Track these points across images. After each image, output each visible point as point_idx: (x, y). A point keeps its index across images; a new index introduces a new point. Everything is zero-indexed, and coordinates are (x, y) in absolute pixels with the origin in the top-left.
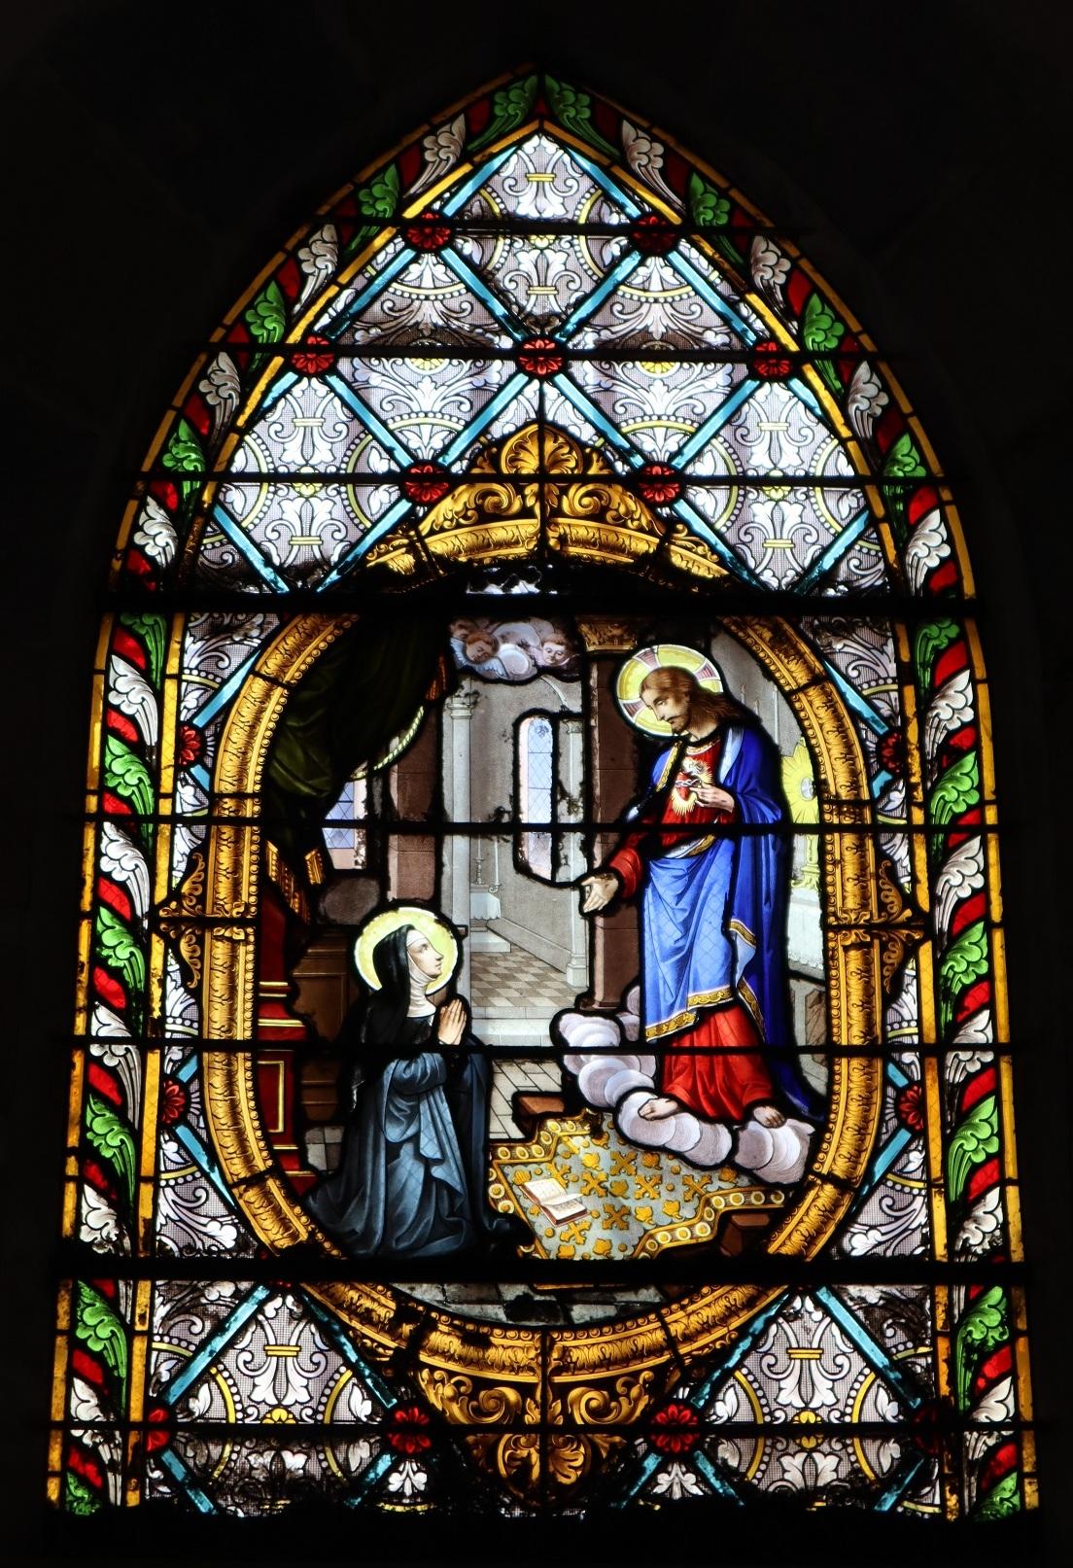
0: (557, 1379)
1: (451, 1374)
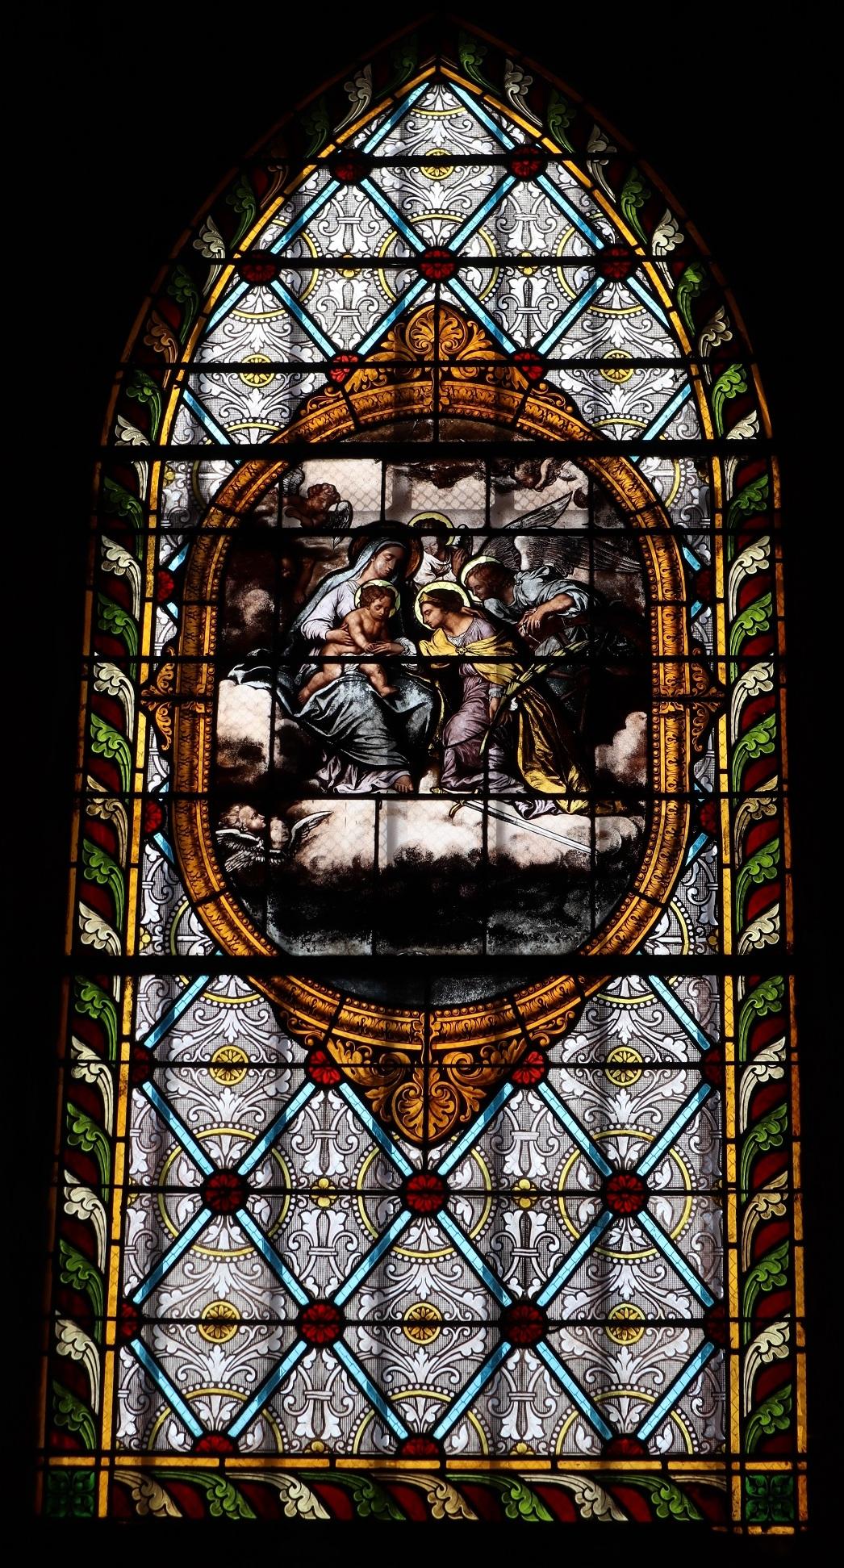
0: (440, 1047)
1: (358, 1043)
